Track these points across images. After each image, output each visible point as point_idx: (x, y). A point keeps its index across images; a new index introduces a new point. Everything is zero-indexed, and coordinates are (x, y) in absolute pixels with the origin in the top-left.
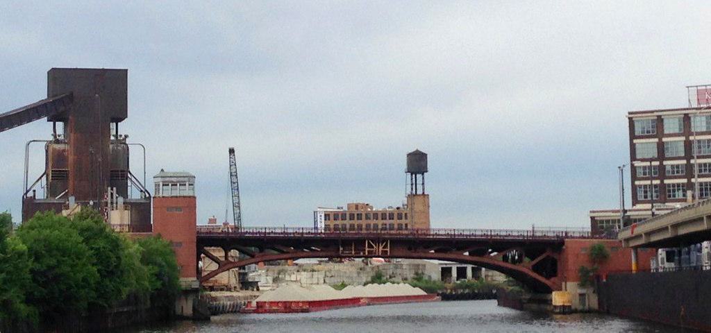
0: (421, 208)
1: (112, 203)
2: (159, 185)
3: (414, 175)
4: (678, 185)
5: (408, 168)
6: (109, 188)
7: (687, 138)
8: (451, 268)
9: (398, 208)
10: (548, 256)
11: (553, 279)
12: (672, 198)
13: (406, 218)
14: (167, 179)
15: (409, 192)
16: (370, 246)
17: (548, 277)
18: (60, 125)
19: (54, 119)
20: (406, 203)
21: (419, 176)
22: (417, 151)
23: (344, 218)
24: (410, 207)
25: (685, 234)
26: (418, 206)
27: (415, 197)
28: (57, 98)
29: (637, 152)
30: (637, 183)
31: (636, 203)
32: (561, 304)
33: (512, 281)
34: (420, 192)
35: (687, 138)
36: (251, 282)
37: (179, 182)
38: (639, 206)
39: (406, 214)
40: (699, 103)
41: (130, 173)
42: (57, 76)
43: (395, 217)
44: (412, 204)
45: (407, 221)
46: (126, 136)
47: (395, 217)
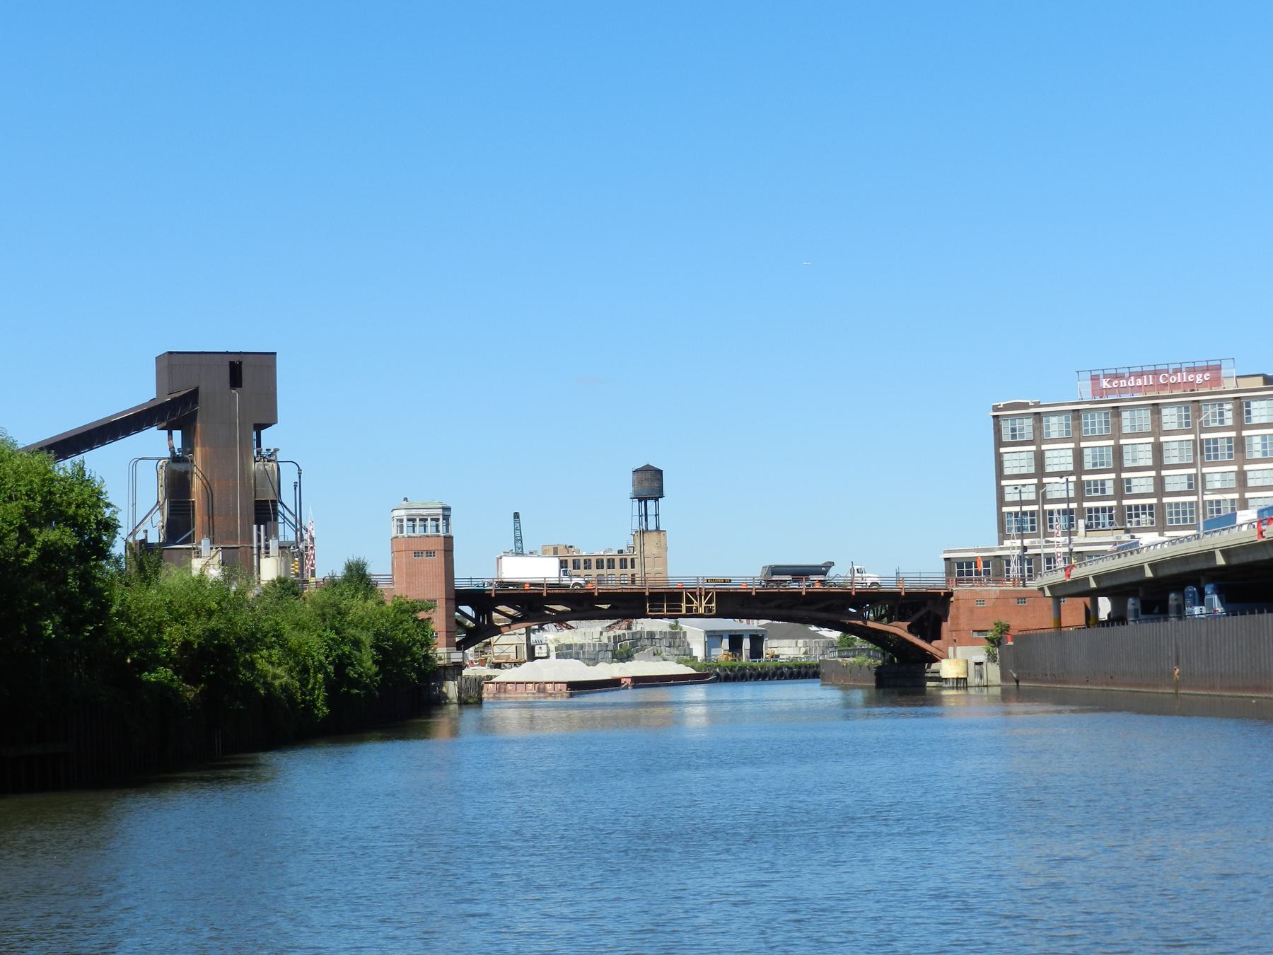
0: (655, 551)
1: (259, 548)
2: (401, 521)
3: (643, 503)
4: (1144, 507)
5: (634, 492)
6: (255, 526)
7: (1241, 467)
8: (1143, 566)
9: (621, 552)
10: (929, 612)
11: (935, 643)
12: (1100, 527)
13: (633, 566)
14: (413, 512)
15: (636, 527)
16: (689, 601)
17: (929, 642)
18: (177, 434)
19: (170, 428)
20: (631, 544)
21: (651, 503)
22: (648, 466)
23: (611, 564)
24: (637, 549)
25: (873, 628)
26: (651, 548)
27: (646, 535)
28: (177, 395)
29: (1006, 464)
30: (1005, 509)
31: (1004, 539)
32: (955, 676)
33: (878, 651)
34: (652, 526)
35: (1241, 467)
36: (445, 667)
37: (429, 515)
38: (1007, 543)
39: (632, 561)
40: (1094, 395)
41: (282, 503)
42: (171, 363)
43: (617, 563)
44: (642, 545)
45: (634, 571)
46: (276, 450)
47: (617, 563)
